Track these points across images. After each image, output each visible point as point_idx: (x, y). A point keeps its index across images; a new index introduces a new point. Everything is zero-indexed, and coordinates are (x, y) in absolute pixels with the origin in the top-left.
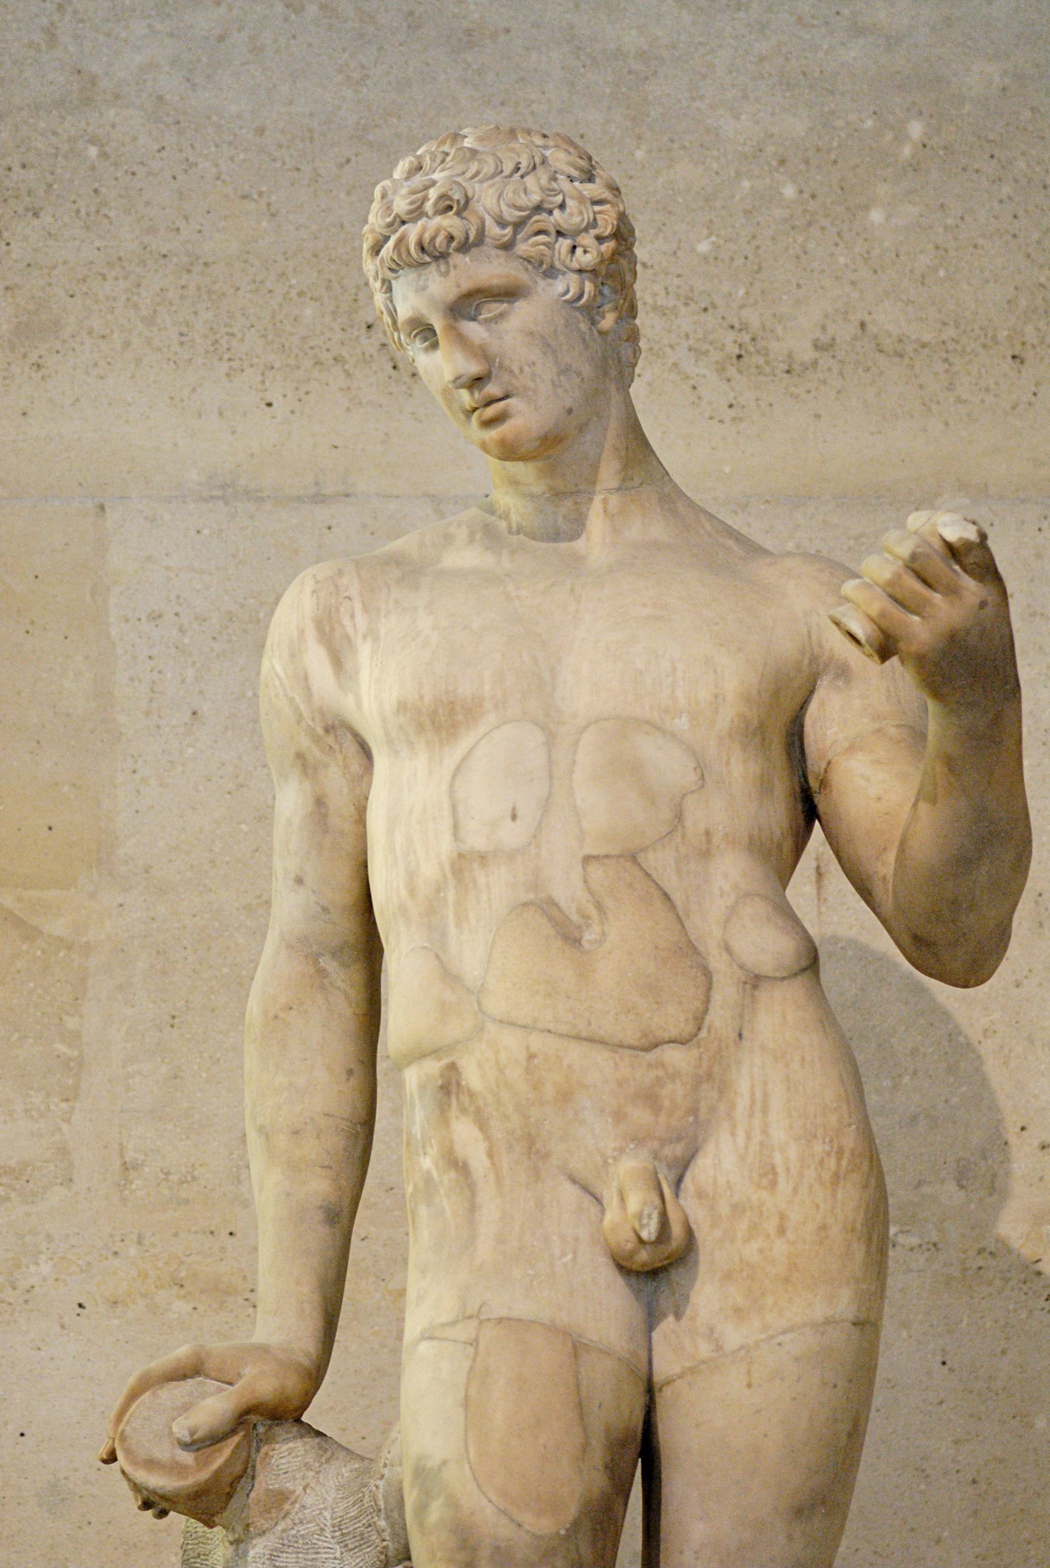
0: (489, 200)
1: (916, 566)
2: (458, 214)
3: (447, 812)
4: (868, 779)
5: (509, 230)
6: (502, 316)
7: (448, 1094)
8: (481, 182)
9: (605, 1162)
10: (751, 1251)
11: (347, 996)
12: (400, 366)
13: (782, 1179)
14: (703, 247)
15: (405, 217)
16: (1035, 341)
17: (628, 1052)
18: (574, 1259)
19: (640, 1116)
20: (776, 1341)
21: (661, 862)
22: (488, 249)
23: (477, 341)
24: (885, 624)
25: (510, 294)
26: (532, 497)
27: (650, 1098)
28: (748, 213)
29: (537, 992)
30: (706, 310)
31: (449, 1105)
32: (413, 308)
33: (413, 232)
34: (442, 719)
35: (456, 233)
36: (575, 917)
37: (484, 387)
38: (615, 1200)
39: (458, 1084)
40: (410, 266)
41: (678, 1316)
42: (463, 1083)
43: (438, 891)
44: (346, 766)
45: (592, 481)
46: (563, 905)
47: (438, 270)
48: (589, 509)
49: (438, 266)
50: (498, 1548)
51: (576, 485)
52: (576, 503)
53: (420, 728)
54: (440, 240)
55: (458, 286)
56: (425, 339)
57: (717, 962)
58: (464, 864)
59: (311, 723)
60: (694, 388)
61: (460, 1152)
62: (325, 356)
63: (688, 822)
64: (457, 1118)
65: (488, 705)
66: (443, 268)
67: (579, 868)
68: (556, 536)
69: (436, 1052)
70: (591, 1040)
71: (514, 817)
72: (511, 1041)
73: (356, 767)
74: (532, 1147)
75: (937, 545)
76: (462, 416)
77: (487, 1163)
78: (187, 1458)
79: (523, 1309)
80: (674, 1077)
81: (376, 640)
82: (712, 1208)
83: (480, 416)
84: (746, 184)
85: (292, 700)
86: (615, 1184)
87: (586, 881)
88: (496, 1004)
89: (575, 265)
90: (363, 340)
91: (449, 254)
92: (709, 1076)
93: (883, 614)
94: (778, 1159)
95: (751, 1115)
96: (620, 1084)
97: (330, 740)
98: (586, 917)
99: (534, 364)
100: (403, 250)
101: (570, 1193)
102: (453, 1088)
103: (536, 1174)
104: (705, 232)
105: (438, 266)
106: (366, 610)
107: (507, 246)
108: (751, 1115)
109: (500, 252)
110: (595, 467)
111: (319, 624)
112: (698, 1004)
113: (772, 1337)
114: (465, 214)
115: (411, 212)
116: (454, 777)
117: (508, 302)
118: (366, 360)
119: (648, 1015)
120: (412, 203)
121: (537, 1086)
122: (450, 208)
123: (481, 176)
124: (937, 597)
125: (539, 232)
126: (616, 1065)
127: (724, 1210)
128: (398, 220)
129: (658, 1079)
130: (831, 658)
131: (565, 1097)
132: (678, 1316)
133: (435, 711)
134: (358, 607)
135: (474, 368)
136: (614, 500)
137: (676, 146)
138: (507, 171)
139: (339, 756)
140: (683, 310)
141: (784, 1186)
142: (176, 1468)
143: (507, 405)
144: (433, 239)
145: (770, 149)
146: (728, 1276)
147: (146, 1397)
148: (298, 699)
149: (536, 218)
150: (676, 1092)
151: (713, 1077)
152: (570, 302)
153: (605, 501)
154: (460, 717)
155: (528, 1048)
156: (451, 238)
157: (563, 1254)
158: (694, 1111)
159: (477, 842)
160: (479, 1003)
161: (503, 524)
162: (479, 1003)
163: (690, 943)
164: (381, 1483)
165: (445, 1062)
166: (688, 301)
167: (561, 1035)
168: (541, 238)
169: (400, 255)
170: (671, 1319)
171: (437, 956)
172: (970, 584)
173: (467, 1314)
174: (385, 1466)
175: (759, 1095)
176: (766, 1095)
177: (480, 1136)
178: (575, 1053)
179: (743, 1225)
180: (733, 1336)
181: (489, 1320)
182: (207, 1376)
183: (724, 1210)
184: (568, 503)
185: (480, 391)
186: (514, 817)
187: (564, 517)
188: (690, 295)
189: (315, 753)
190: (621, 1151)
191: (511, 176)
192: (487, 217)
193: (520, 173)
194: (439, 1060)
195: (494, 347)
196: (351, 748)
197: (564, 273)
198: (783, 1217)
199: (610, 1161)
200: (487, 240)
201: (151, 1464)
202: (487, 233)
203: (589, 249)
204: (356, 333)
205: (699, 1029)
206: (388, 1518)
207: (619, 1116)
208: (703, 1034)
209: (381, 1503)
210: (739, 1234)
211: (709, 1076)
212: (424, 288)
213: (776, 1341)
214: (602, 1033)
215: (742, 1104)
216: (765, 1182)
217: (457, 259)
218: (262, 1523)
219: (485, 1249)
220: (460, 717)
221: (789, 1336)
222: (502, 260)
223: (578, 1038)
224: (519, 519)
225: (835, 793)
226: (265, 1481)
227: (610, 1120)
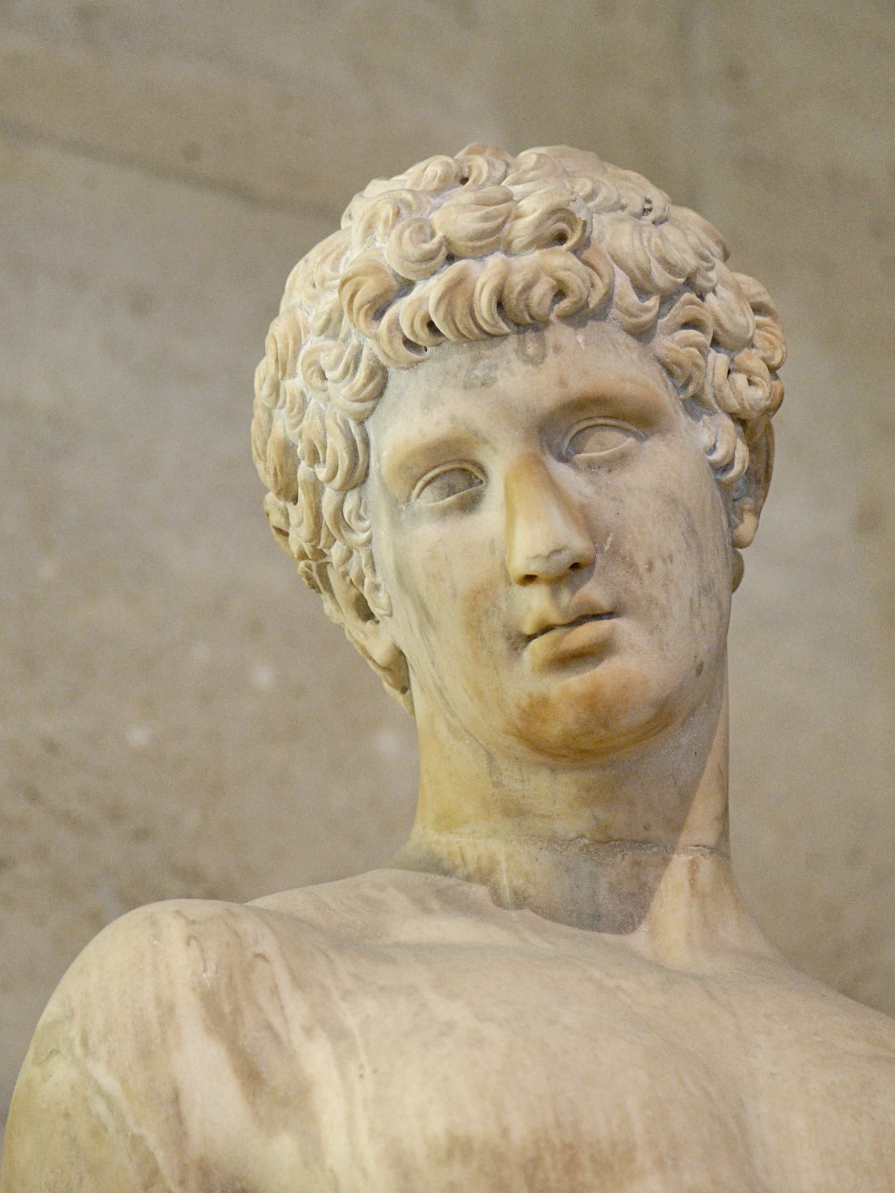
6: (621, 460)
15: (461, 245)
22: (611, 330)
23: (576, 498)
25: (642, 421)
26: (553, 841)
32: (453, 419)
33: (485, 275)
37: (583, 583)
45: (676, 827)
47: (521, 351)
48: (659, 878)
49: (522, 344)
51: (646, 828)
52: (637, 863)
54: (542, 291)
55: (562, 383)
65: (644, 1159)
66: (531, 348)
68: (592, 920)
76: (501, 646)
81: (339, 1035)
83: (559, 640)
85: (136, 1142)
91: (547, 323)
99: (671, 558)
100: (460, 303)
105: (522, 344)
106: (299, 984)
107: (642, 334)
109: (632, 342)
110: (686, 799)
111: (209, 999)
114: (587, 254)
115: (481, 235)
117: (635, 435)
120: (486, 218)
122: (561, 238)
123: (598, 200)
128: (444, 251)
133: (537, 1161)
134: (283, 978)
135: (578, 544)
143: (614, 629)
144: (528, 287)
148: (151, 1141)
153: (694, 866)
161: (480, 892)
166: (115, 815)
169: (450, 316)
184: (620, 865)
185: (573, 592)
187: (612, 887)
193: (651, 216)
195: (606, 513)
197: (712, 412)
200: (614, 312)
202: (616, 299)
203: (757, 379)
217: (560, 334)
222: (634, 356)
224: (519, 882)
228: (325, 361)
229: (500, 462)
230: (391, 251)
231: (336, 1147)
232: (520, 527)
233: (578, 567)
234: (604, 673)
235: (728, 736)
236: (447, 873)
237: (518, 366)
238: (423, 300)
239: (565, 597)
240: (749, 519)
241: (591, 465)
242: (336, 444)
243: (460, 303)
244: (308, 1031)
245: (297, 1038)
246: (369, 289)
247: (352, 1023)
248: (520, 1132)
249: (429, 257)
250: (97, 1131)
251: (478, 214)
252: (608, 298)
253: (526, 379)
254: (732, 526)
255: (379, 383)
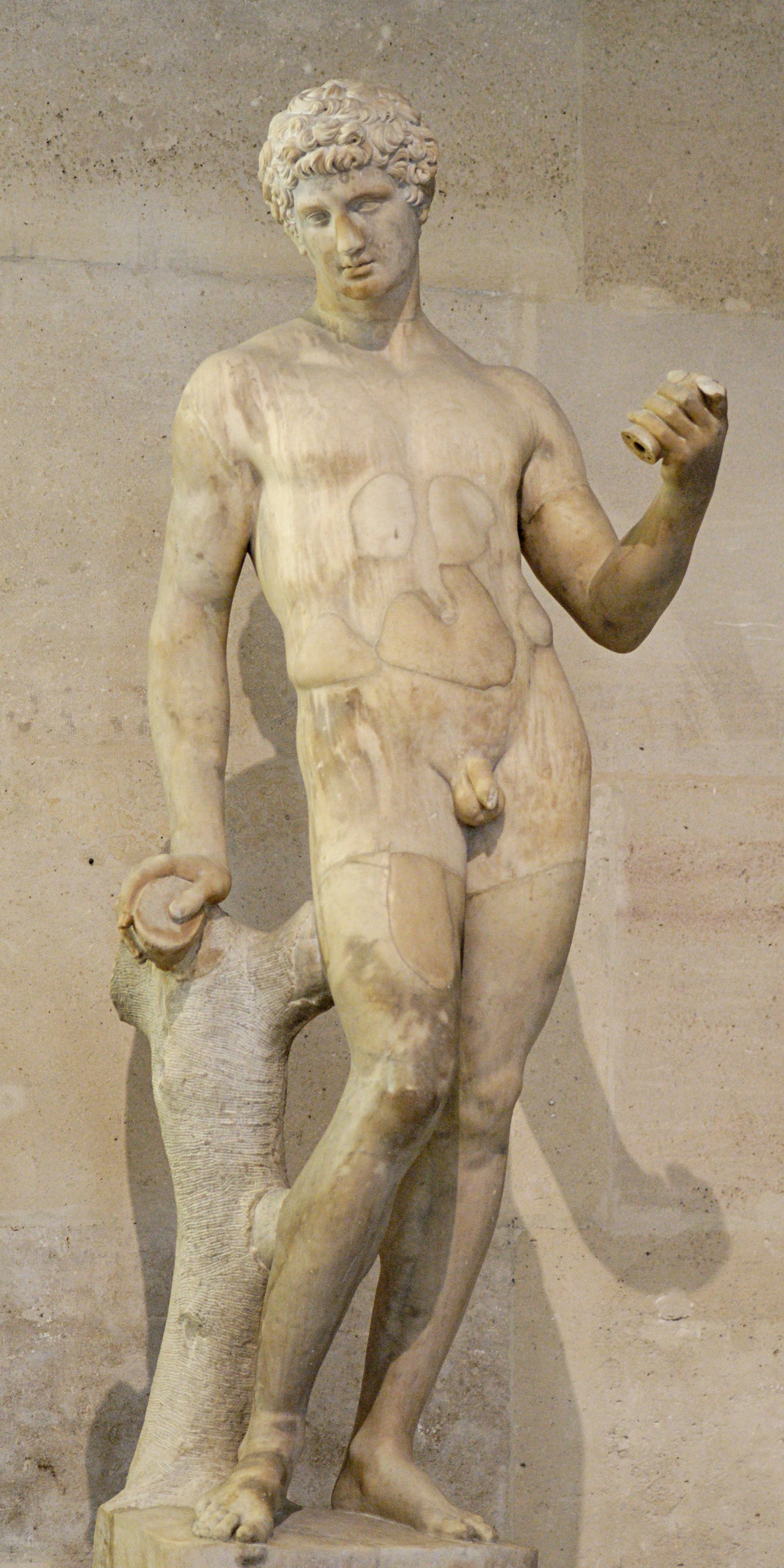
0: (377, 137)
1: (687, 409)
2: (360, 145)
3: (348, 528)
4: (569, 518)
5: (386, 157)
6: (375, 211)
7: (353, 708)
8: (370, 124)
9: (456, 756)
10: (537, 816)
11: (217, 630)
12: (67, 171)
13: (554, 773)
14: (255, 103)
15: (321, 143)
16: (454, 182)
17: (473, 690)
18: (437, 817)
19: (478, 730)
20: (548, 872)
21: (480, 568)
22: (373, 168)
24: (664, 441)
26: (357, 320)
27: (484, 719)
28: (282, 81)
29: (420, 650)
30: (255, 146)
31: (354, 715)
32: (318, 200)
33: (329, 153)
34: (337, 469)
35: (359, 158)
36: (436, 602)
38: (464, 781)
39: (360, 702)
40: (321, 174)
41: (488, 853)
42: (364, 702)
43: (342, 578)
44: (243, 486)
45: (398, 314)
46: (430, 594)
47: (341, 179)
50: (415, 995)
52: (385, 327)
53: (323, 472)
54: (347, 161)
55: (354, 190)
56: (319, 219)
57: (517, 635)
58: (361, 564)
59: (225, 458)
60: (247, 199)
61: (362, 745)
62: (22, 161)
63: (492, 545)
64: (360, 724)
66: (344, 178)
67: (438, 572)
68: (371, 347)
69: (345, 681)
70: (453, 681)
71: (396, 536)
72: (401, 680)
73: (248, 487)
74: (409, 747)
75: (696, 393)
76: (335, 269)
77: (380, 753)
78: (177, 928)
79: (414, 846)
80: (498, 706)
81: (278, 410)
82: (514, 789)
84: (282, 61)
85: (213, 443)
86: (463, 771)
87: (442, 581)
88: (390, 653)
89: (417, 181)
90: (45, 152)
92: (515, 706)
93: (665, 436)
94: (552, 760)
95: (536, 732)
96: (468, 709)
97: (236, 469)
98: (443, 603)
100: (320, 165)
101: (431, 774)
102: (357, 704)
103: (411, 762)
104: (256, 92)
106: (266, 388)
107: (383, 167)
108: (536, 732)
109: (379, 171)
110: (402, 306)
111: (236, 395)
112: (510, 662)
113: (547, 870)
114: (363, 145)
116: (351, 506)
118: (46, 165)
119: (486, 667)
121: (417, 708)
122: (355, 141)
123: (370, 119)
124: (696, 427)
125: (403, 159)
126: (467, 698)
127: (522, 790)
129: (490, 708)
130: (543, 438)
131: (435, 715)
132: (488, 853)
134: (261, 386)
135: (358, 243)
136: (409, 326)
137: (240, 32)
138: (383, 118)
139: (240, 480)
140: (242, 145)
141: (556, 777)
142: (173, 935)
144: (343, 160)
145: (297, 39)
146: (522, 831)
147: (146, 888)
149: (400, 150)
150: (497, 715)
151: (516, 708)
152: (410, 204)
153: (404, 327)
154: (351, 468)
155: (412, 684)
156: (354, 160)
157: (432, 814)
158: (506, 728)
159: (371, 548)
160: (378, 653)
161: (333, 335)
162: (378, 653)
163: (503, 622)
164: (293, 949)
165: (350, 688)
167: (435, 677)
168: (402, 163)
169: (317, 167)
170: (483, 855)
171: (343, 620)
172: (713, 420)
173: (382, 848)
174: (297, 937)
175: (539, 719)
176: (543, 719)
177: (376, 736)
178: (443, 690)
179: (532, 800)
180: (523, 868)
181: (396, 853)
182: (177, 876)
183: (522, 790)
184: (380, 327)
186: (396, 536)
188: (246, 135)
189: (225, 476)
190: (466, 751)
191: (385, 121)
192: (374, 148)
194: (346, 686)
196: (247, 475)
197: (409, 185)
198: (555, 797)
199: (459, 757)
200: (373, 163)
201: (157, 931)
204: (40, 146)
205: (512, 677)
206: (297, 969)
207: (466, 729)
208: (513, 681)
209: (293, 961)
210: (530, 806)
211: (515, 706)
212: (329, 189)
213: (548, 872)
214: (459, 677)
215: (531, 724)
216: (545, 774)
217: (354, 173)
218: (202, 969)
219: (385, 806)
220: (351, 468)
221: (556, 870)
223: (446, 680)
225: (545, 526)
226: (208, 944)
227: (460, 731)
228: (280, 169)
229: (335, 214)
230: (297, 138)
231: (275, 450)
232: (339, 238)
233: (359, 251)
234: (368, 281)
235: (229, 713)
236: (323, 326)
237: (339, 183)
238: (308, 161)
239: (355, 259)
240: (425, 212)
241: (365, 213)
242: (283, 195)
243: (320, 165)
244: (268, 407)
245: (264, 409)
246: (291, 154)
247: (282, 404)
248: (330, 454)
249: (310, 147)
250: (201, 438)
251: (327, 133)
252: (371, 159)
253: (342, 189)
254: (417, 216)
255: (295, 182)
